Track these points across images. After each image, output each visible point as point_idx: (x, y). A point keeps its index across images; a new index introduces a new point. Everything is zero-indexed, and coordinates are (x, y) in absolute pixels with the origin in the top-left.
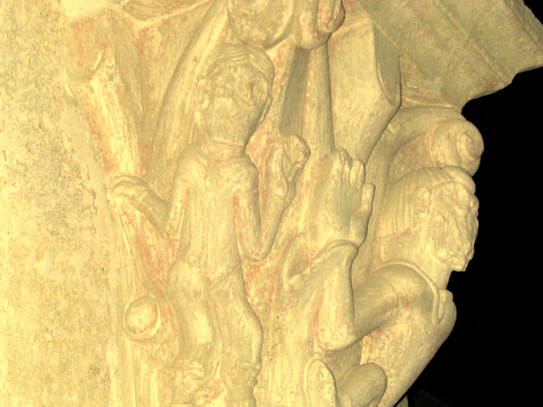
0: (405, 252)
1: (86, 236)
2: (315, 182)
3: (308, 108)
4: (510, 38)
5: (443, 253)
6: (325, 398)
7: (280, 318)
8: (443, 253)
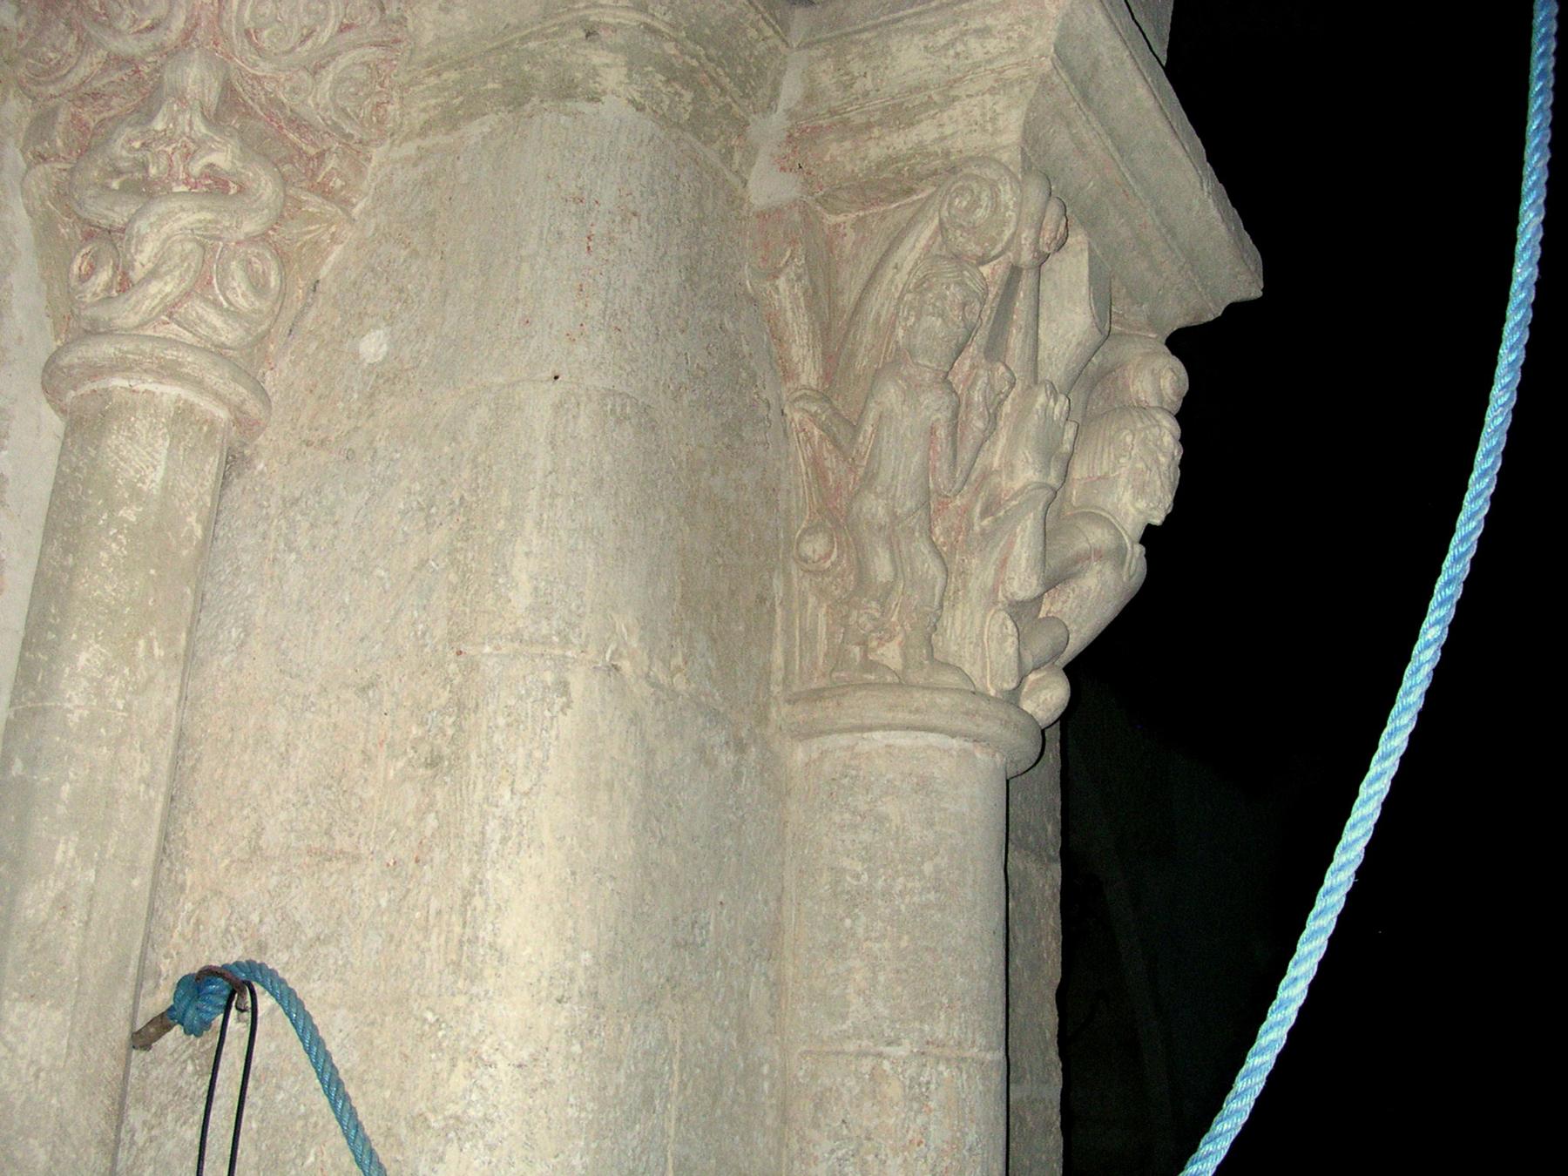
5: (1141, 504)
8: (1141, 504)
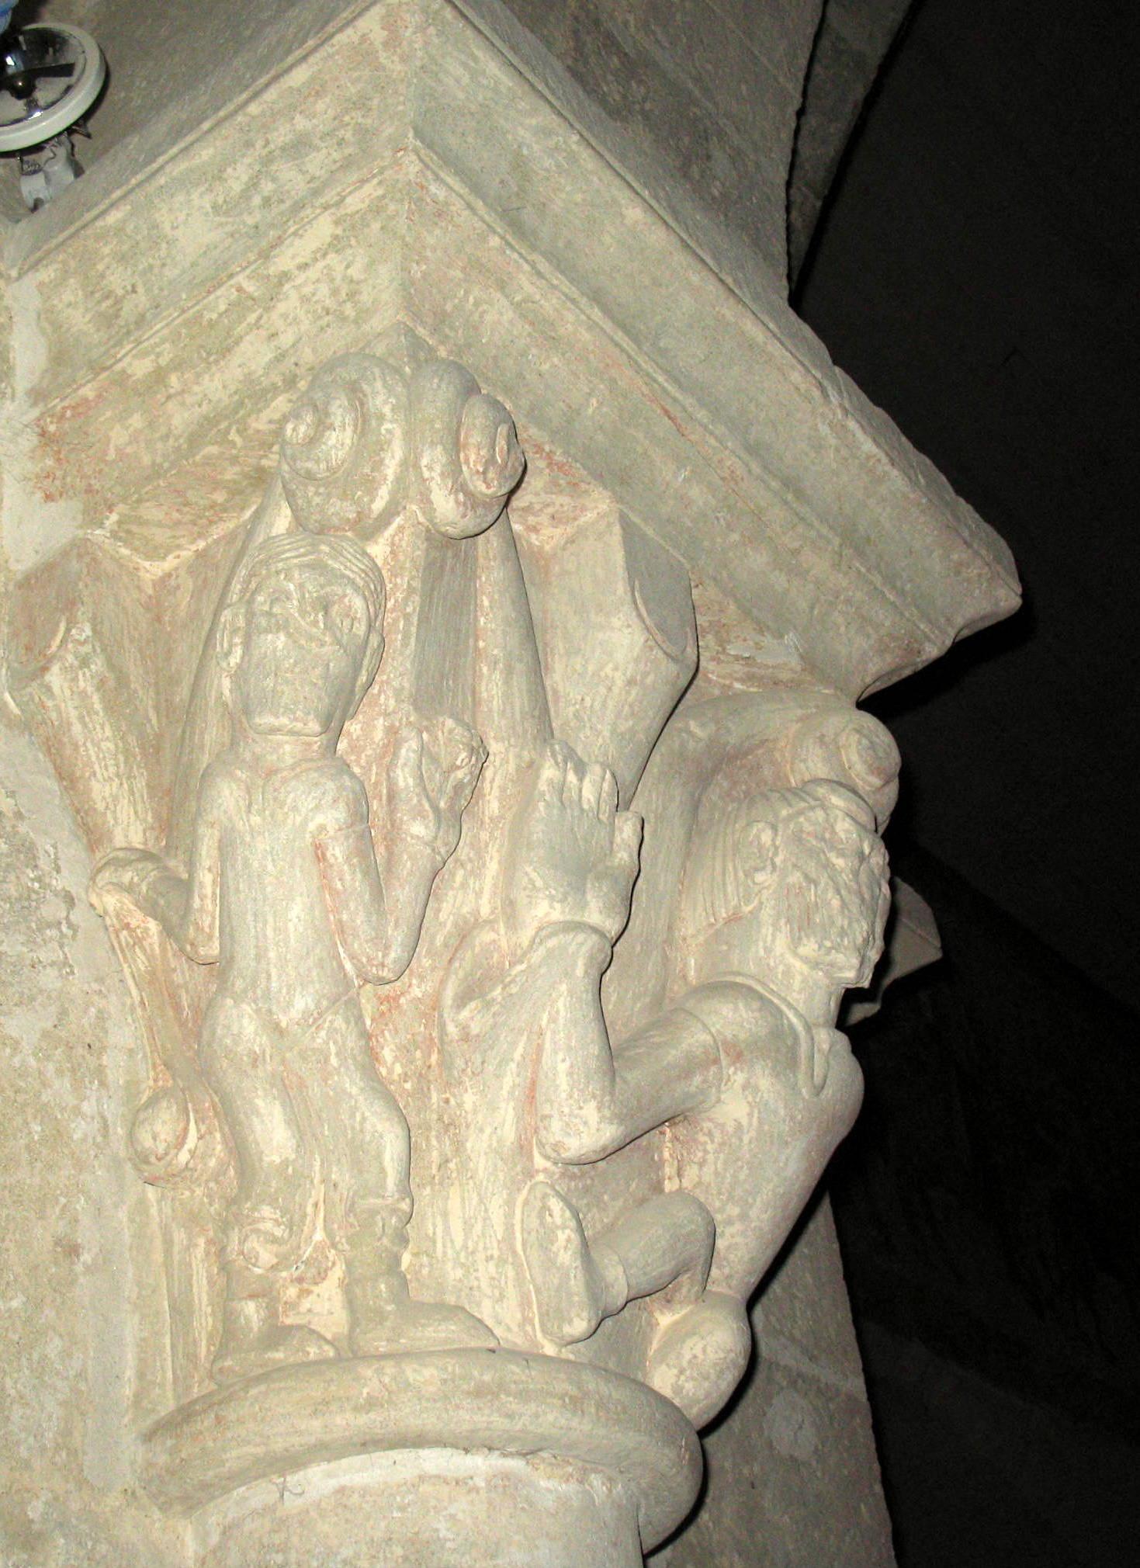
0: (735, 957)
1: (49, 979)
2: (509, 816)
3: (485, 670)
4: (932, 552)
5: (809, 948)
6: (560, 1260)
7: (452, 1102)
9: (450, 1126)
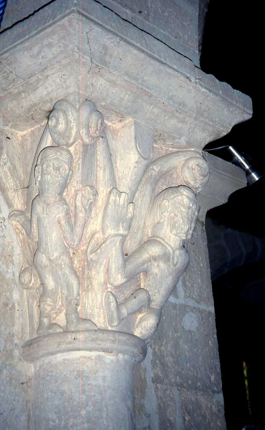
3: (99, 169)
9: (89, 278)
